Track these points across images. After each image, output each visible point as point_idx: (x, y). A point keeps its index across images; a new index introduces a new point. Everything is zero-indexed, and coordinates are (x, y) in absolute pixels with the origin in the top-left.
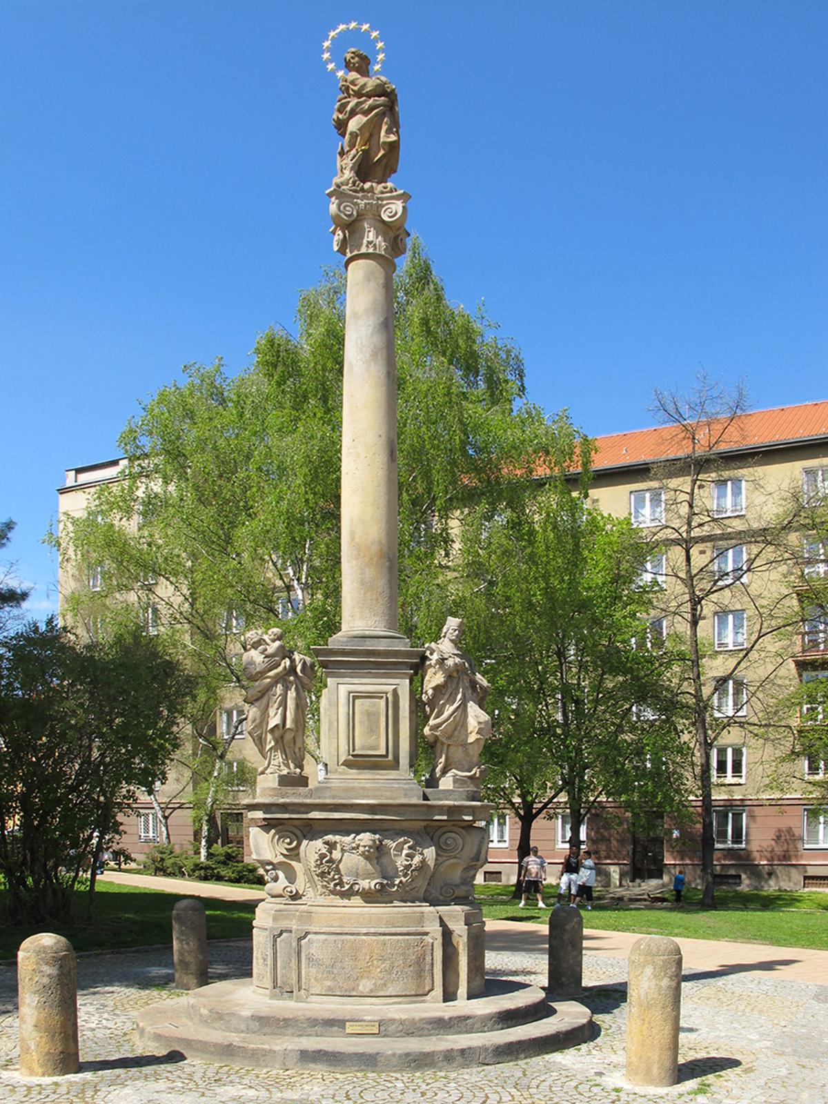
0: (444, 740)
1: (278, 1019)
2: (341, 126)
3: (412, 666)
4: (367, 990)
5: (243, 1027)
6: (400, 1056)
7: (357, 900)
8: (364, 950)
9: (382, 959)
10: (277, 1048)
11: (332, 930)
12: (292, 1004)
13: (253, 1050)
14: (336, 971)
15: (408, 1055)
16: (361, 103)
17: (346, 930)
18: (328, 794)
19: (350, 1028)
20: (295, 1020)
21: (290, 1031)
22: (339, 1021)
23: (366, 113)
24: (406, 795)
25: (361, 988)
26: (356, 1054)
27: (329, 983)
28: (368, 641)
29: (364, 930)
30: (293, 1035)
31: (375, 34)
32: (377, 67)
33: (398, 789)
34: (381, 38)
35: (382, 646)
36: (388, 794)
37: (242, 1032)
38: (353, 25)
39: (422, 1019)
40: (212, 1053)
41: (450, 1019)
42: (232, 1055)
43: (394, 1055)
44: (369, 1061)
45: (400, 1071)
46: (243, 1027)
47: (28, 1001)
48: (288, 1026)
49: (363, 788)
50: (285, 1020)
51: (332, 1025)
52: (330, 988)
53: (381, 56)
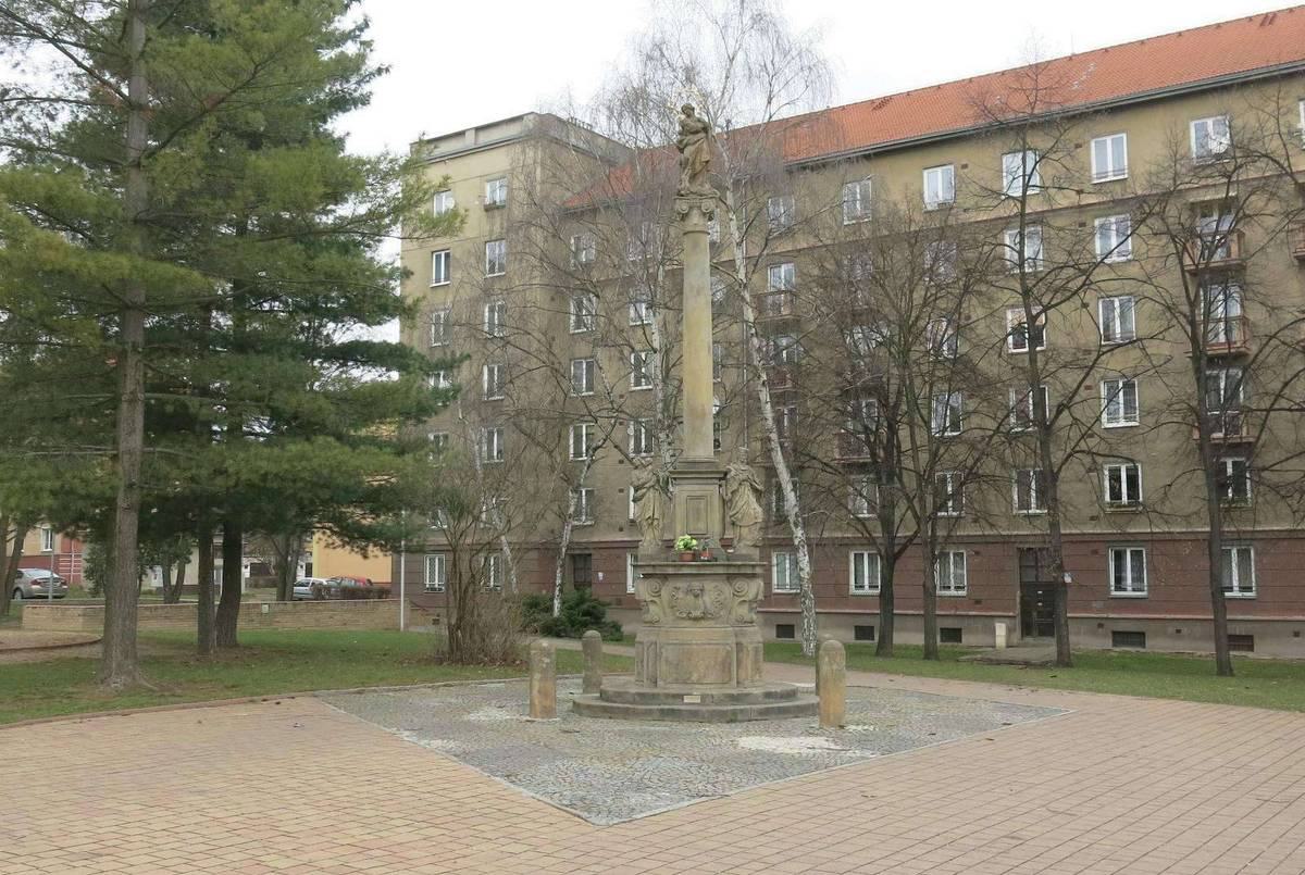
5: (631, 700)
46: (631, 700)
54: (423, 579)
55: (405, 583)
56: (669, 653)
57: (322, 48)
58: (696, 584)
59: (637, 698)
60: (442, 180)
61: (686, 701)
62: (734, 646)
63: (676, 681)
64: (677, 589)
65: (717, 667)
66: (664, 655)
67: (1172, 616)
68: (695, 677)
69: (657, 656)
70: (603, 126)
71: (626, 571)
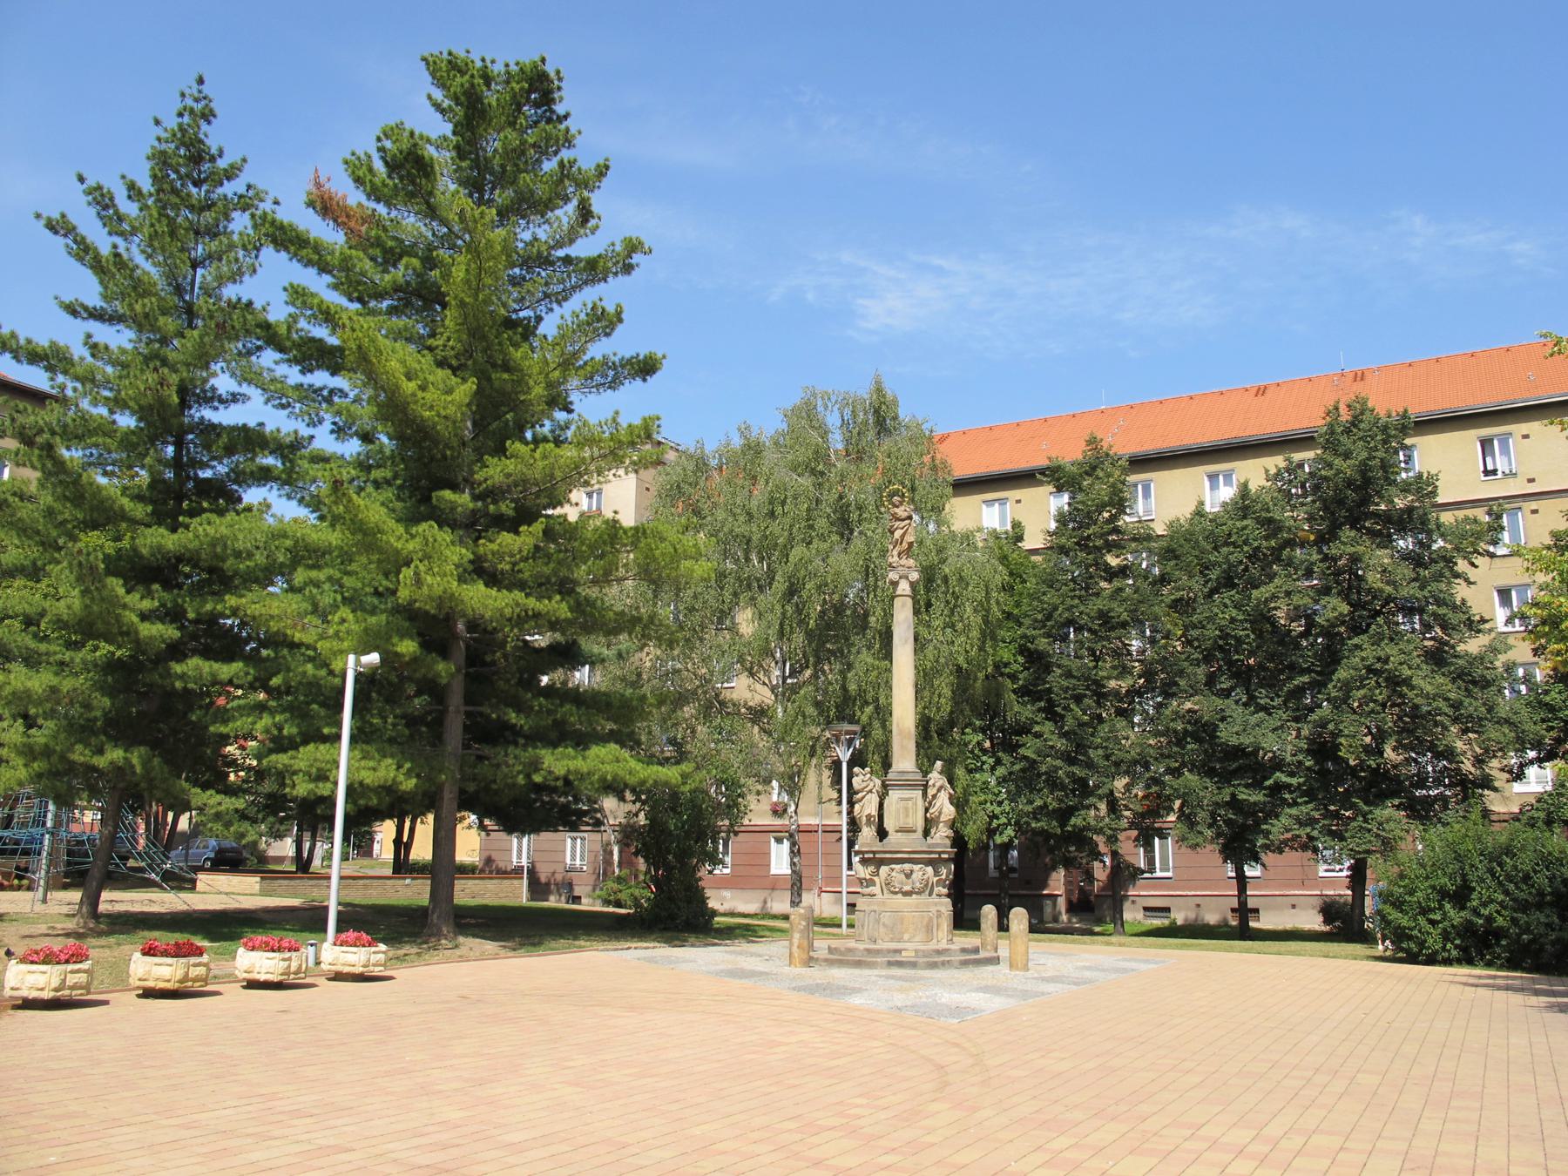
44: (913, 965)
56: (885, 918)
58: (907, 866)
68: (906, 937)
69: (878, 921)
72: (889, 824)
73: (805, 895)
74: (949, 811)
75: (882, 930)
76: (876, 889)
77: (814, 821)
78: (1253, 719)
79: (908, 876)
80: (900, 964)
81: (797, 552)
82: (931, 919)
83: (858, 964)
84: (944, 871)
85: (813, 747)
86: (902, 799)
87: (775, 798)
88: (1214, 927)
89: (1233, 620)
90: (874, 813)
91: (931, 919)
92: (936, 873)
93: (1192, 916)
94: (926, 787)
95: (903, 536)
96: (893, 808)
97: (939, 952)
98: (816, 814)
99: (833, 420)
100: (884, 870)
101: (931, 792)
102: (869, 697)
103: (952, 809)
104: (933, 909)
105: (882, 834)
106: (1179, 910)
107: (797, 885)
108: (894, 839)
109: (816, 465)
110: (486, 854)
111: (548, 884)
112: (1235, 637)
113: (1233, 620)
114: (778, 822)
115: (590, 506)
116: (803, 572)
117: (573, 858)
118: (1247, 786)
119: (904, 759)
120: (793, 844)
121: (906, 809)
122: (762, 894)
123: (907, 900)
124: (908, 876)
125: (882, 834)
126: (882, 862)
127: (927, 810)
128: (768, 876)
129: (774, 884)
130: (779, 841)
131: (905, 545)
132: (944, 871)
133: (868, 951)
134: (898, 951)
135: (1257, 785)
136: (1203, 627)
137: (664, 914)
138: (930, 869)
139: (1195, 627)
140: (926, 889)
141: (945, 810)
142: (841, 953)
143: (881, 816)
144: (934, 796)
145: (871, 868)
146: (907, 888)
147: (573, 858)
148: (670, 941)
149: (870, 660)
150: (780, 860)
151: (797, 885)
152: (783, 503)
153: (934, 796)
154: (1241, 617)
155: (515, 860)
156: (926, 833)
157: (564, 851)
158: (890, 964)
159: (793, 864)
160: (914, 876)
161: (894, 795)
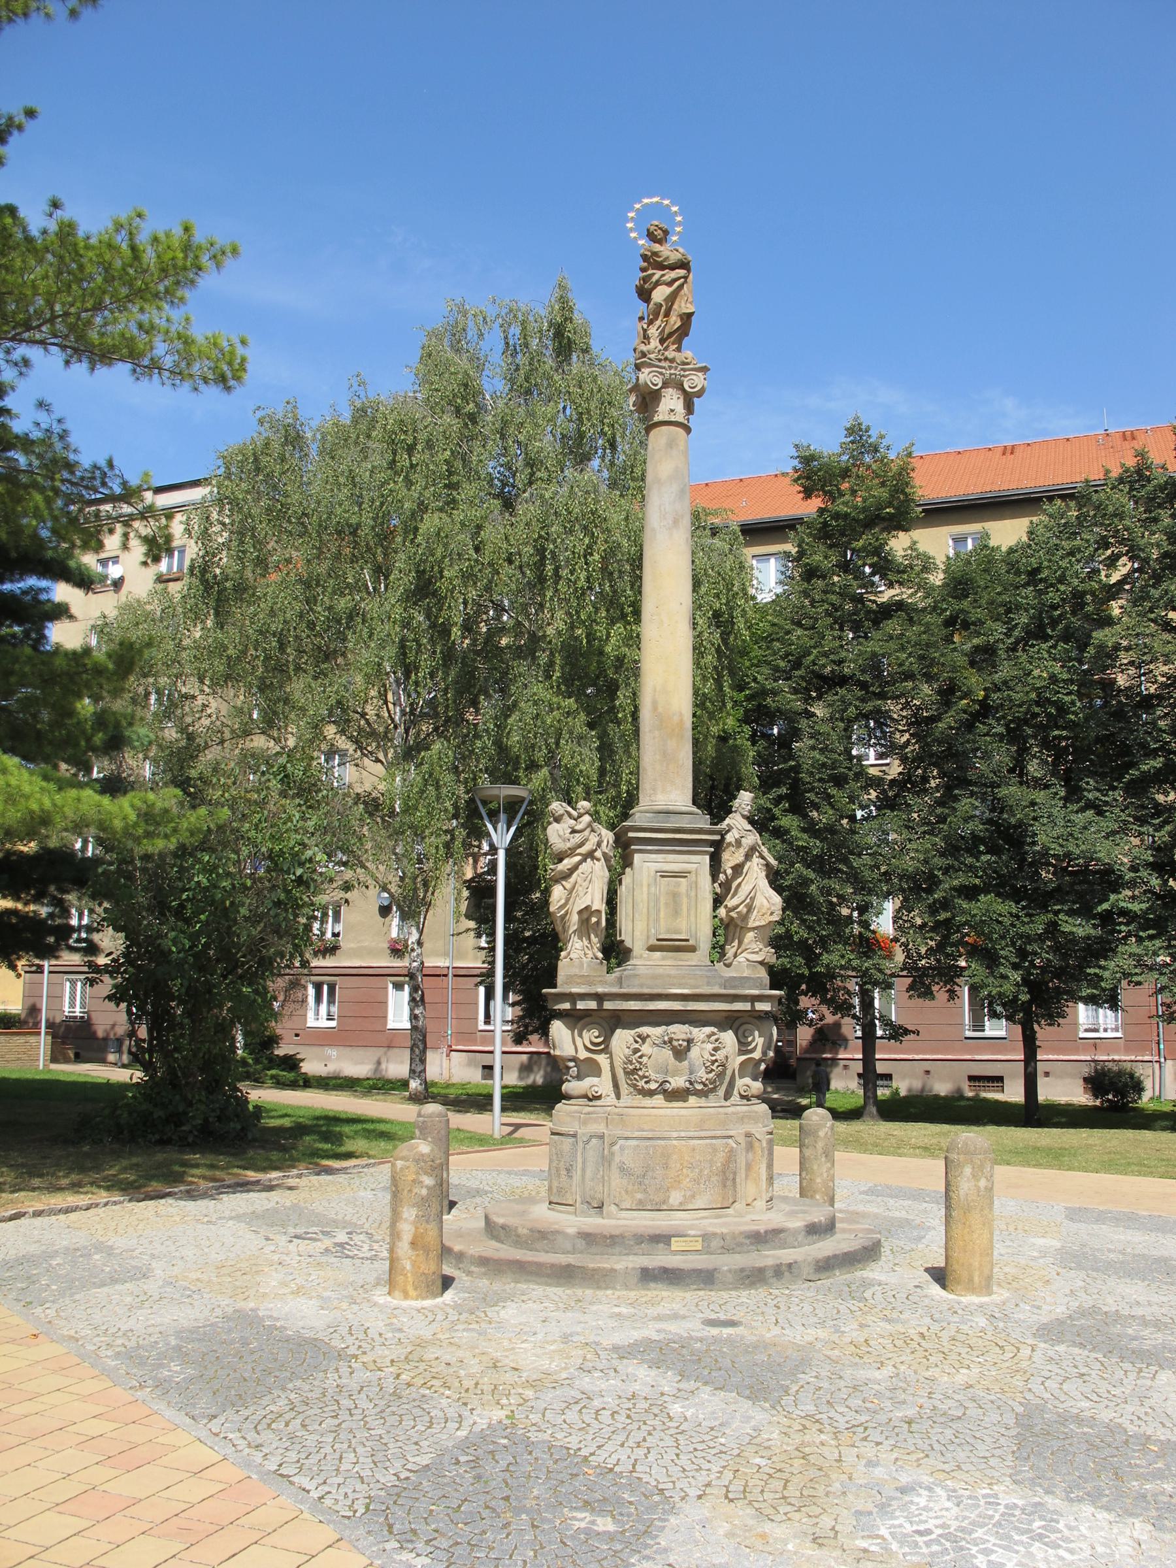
0: (739, 922)
1: (605, 1236)
2: (644, 294)
3: (712, 843)
4: (677, 1203)
5: (569, 1247)
6: (735, 1271)
7: (659, 1100)
8: (675, 1157)
9: (692, 1167)
10: (618, 1267)
11: (645, 1134)
12: (598, 1221)
13: (594, 1270)
14: (647, 1182)
15: (742, 1270)
16: (663, 275)
17: (658, 1134)
18: (637, 982)
19: (676, 1244)
20: (622, 1236)
21: (617, 1249)
22: (665, 1236)
23: (670, 284)
24: (708, 984)
25: (671, 1200)
26: (694, 1270)
27: (639, 1196)
28: (673, 817)
29: (675, 1134)
30: (620, 1254)
31: (675, 209)
32: (675, 238)
33: (701, 976)
34: (680, 213)
35: (684, 823)
36: (692, 982)
37: (568, 1252)
38: (666, 202)
39: (741, 1233)
40: (548, 1276)
41: (766, 1232)
42: (570, 1277)
43: (730, 1271)
44: (706, 1278)
45: (736, 1289)
46: (569, 1247)
47: (405, 1215)
48: (615, 1244)
49: (669, 976)
50: (612, 1237)
51: (658, 1242)
52: (640, 1202)
53: (637, 206)
54: (62, 1005)
55: (477, 1004)
56: (626, 1154)
57: (29, 239)
58: (679, 1031)
59: (581, 1244)
60: (111, 226)
61: (673, 1248)
62: (742, 1140)
63: (641, 1207)
64: (643, 1038)
65: (714, 1179)
66: (617, 1159)
67: (1055, 1057)
68: (675, 1198)
69: (606, 1160)
70: (522, 1083)
71: (386, 1003)
72: (634, 930)
73: (430, 1056)
74: (768, 904)
75: (617, 1181)
76: (601, 1084)
77: (443, 963)
78: (1080, 819)
79: (680, 1053)
80: (671, 1277)
81: (430, 523)
82: (731, 1155)
83: (565, 1275)
84: (758, 1041)
85: (447, 845)
86: (665, 875)
87: (394, 934)
88: (945, 1098)
89: (1053, 679)
90: (599, 905)
91: (731, 1155)
92: (744, 1046)
93: (917, 1085)
94: (716, 851)
95: (672, 298)
96: (642, 895)
97: (760, 1239)
98: (446, 954)
99: (492, 346)
100: (622, 1039)
101: (730, 859)
102: (540, 755)
103: (777, 900)
104: (738, 1131)
105: (614, 951)
106: (903, 1078)
107: (419, 1042)
108: (647, 969)
109: (464, 401)
110: (30, 1001)
111: (105, 1039)
112: (1054, 703)
113: (1053, 679)
114: (397, 963)
115: (170, 567)
116: (439, 552)
117: (72, 1004)
118: (1071, 913)
119: (666, 784)
120: (415, 989)
121: (675, 896)
122: (373, 1054)
123: (676, 1109)
124: (680, 1053)
125: (614, 951)
126: (617, 1020)
127: (718, 901)
128: (384, 1031)
129: (390, 1041)
130: (398, 987)
131: (675, 321)
132: (758, 1041)
133: (589, 1238)
134: (661, 1239)
135: (1086, 912)
136: (1010, 689)
137: (159, 1113)
138: (728, 1038)
139: (997, 689)
140: (716, 1085)
141: (760, 901)
142: (519, 1241)
143: (612, 922)
144: (738, 869)
145: (591, 1035)
146: (678, 1082)
147: (72, 1004)
148: (135, 1190)
149: (547, 695)
150: (398, 1011)
151: (419, 1042)
152: (411, 449)
153: (738, 869)
154: (1065, 676)
155: (67, 1009)
156: (719, 950)
157: (61, 997)
158: (648, 1276)
159: (414, 1017)
160: (694, 1052)
161: (646, 864)
